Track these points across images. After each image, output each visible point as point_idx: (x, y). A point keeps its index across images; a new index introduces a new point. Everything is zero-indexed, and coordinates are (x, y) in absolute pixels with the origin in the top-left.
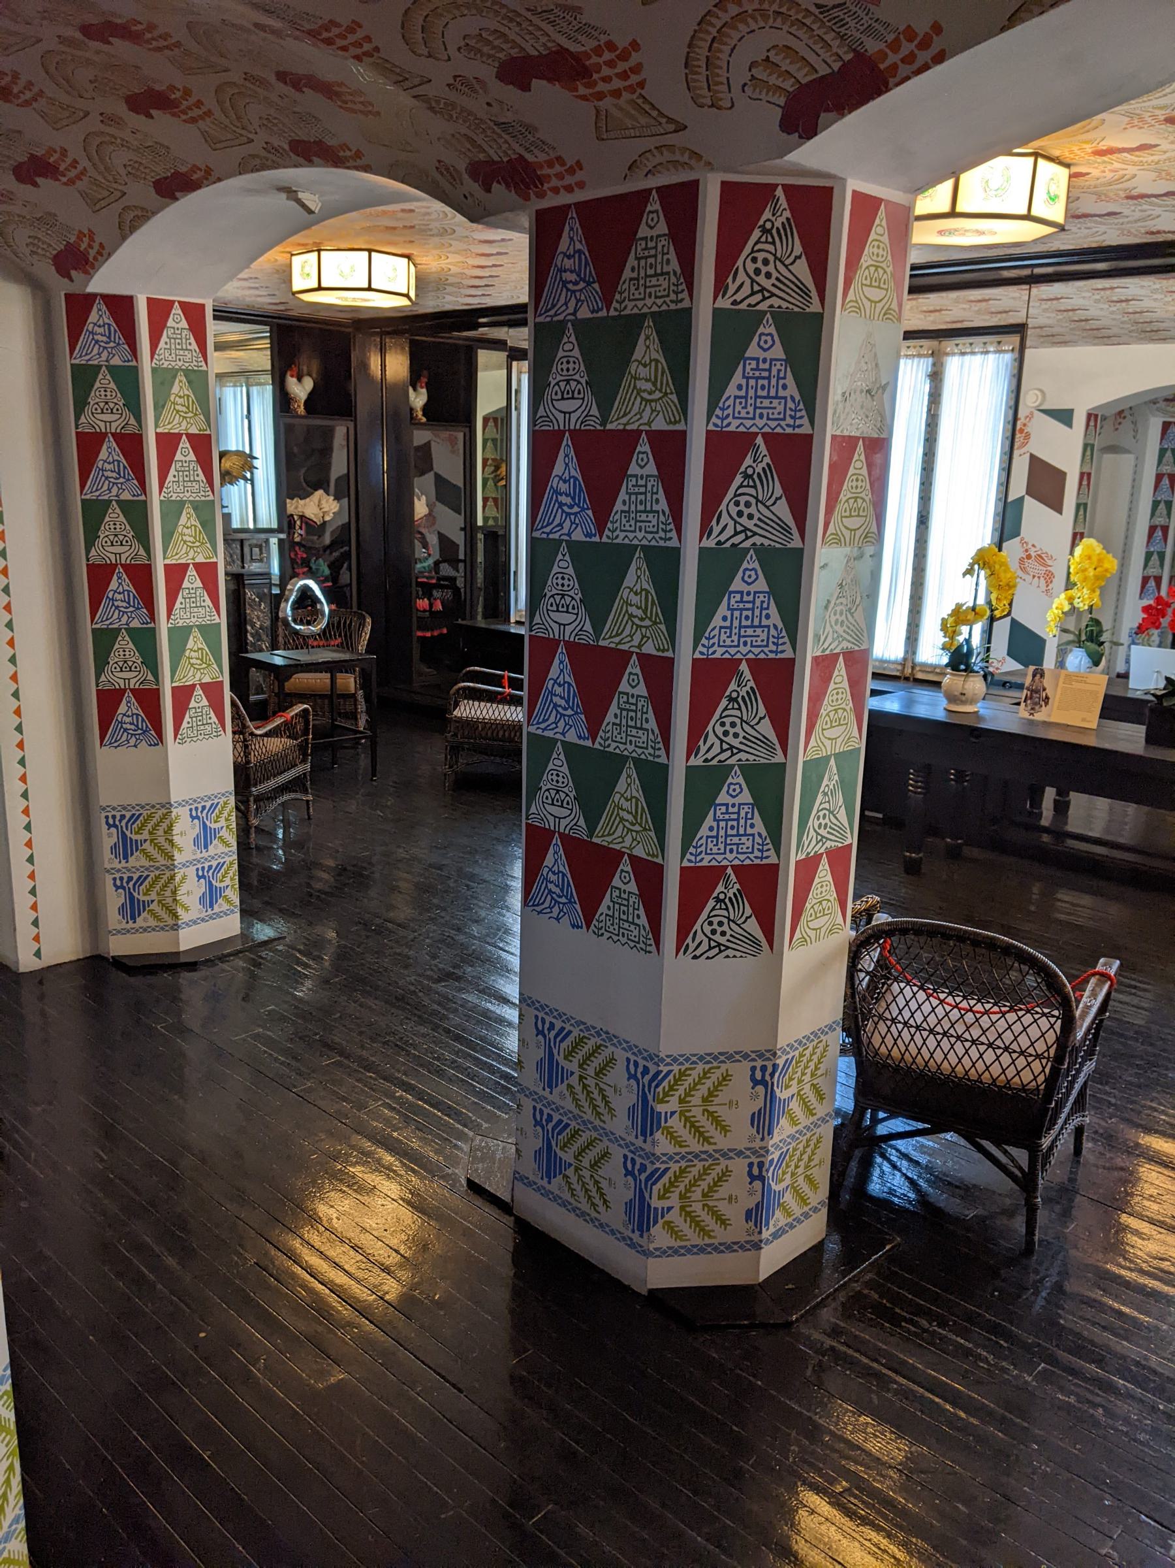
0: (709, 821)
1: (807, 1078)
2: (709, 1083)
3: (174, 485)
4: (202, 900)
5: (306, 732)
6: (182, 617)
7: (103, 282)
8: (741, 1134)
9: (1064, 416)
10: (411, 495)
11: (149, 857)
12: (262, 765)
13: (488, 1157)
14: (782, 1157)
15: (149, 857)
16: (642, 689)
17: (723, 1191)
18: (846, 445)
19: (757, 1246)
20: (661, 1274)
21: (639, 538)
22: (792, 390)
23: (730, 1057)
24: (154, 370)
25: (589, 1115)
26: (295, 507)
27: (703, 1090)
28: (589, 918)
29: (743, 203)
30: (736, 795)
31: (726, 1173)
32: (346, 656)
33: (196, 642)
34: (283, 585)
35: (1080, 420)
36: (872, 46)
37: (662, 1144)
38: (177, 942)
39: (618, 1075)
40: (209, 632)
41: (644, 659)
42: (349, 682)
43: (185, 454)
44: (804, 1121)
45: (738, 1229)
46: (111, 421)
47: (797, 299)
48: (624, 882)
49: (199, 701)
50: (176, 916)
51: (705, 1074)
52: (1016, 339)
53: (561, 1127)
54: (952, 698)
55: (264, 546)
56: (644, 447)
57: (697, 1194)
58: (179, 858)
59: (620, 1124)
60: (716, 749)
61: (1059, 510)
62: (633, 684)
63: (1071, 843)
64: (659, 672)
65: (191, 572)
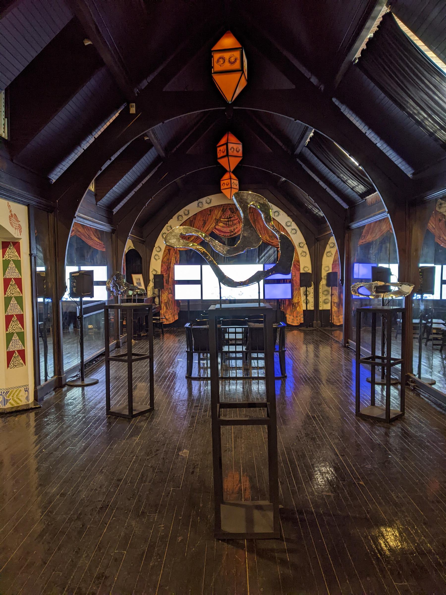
0: (10, 307)
2: (17, 392)
17: (20, 395)
27: (16, 394)
31: (20, 391)
47: (20, 330)
51: (16, 390)
57: (15, 396)
60: (9, 294)
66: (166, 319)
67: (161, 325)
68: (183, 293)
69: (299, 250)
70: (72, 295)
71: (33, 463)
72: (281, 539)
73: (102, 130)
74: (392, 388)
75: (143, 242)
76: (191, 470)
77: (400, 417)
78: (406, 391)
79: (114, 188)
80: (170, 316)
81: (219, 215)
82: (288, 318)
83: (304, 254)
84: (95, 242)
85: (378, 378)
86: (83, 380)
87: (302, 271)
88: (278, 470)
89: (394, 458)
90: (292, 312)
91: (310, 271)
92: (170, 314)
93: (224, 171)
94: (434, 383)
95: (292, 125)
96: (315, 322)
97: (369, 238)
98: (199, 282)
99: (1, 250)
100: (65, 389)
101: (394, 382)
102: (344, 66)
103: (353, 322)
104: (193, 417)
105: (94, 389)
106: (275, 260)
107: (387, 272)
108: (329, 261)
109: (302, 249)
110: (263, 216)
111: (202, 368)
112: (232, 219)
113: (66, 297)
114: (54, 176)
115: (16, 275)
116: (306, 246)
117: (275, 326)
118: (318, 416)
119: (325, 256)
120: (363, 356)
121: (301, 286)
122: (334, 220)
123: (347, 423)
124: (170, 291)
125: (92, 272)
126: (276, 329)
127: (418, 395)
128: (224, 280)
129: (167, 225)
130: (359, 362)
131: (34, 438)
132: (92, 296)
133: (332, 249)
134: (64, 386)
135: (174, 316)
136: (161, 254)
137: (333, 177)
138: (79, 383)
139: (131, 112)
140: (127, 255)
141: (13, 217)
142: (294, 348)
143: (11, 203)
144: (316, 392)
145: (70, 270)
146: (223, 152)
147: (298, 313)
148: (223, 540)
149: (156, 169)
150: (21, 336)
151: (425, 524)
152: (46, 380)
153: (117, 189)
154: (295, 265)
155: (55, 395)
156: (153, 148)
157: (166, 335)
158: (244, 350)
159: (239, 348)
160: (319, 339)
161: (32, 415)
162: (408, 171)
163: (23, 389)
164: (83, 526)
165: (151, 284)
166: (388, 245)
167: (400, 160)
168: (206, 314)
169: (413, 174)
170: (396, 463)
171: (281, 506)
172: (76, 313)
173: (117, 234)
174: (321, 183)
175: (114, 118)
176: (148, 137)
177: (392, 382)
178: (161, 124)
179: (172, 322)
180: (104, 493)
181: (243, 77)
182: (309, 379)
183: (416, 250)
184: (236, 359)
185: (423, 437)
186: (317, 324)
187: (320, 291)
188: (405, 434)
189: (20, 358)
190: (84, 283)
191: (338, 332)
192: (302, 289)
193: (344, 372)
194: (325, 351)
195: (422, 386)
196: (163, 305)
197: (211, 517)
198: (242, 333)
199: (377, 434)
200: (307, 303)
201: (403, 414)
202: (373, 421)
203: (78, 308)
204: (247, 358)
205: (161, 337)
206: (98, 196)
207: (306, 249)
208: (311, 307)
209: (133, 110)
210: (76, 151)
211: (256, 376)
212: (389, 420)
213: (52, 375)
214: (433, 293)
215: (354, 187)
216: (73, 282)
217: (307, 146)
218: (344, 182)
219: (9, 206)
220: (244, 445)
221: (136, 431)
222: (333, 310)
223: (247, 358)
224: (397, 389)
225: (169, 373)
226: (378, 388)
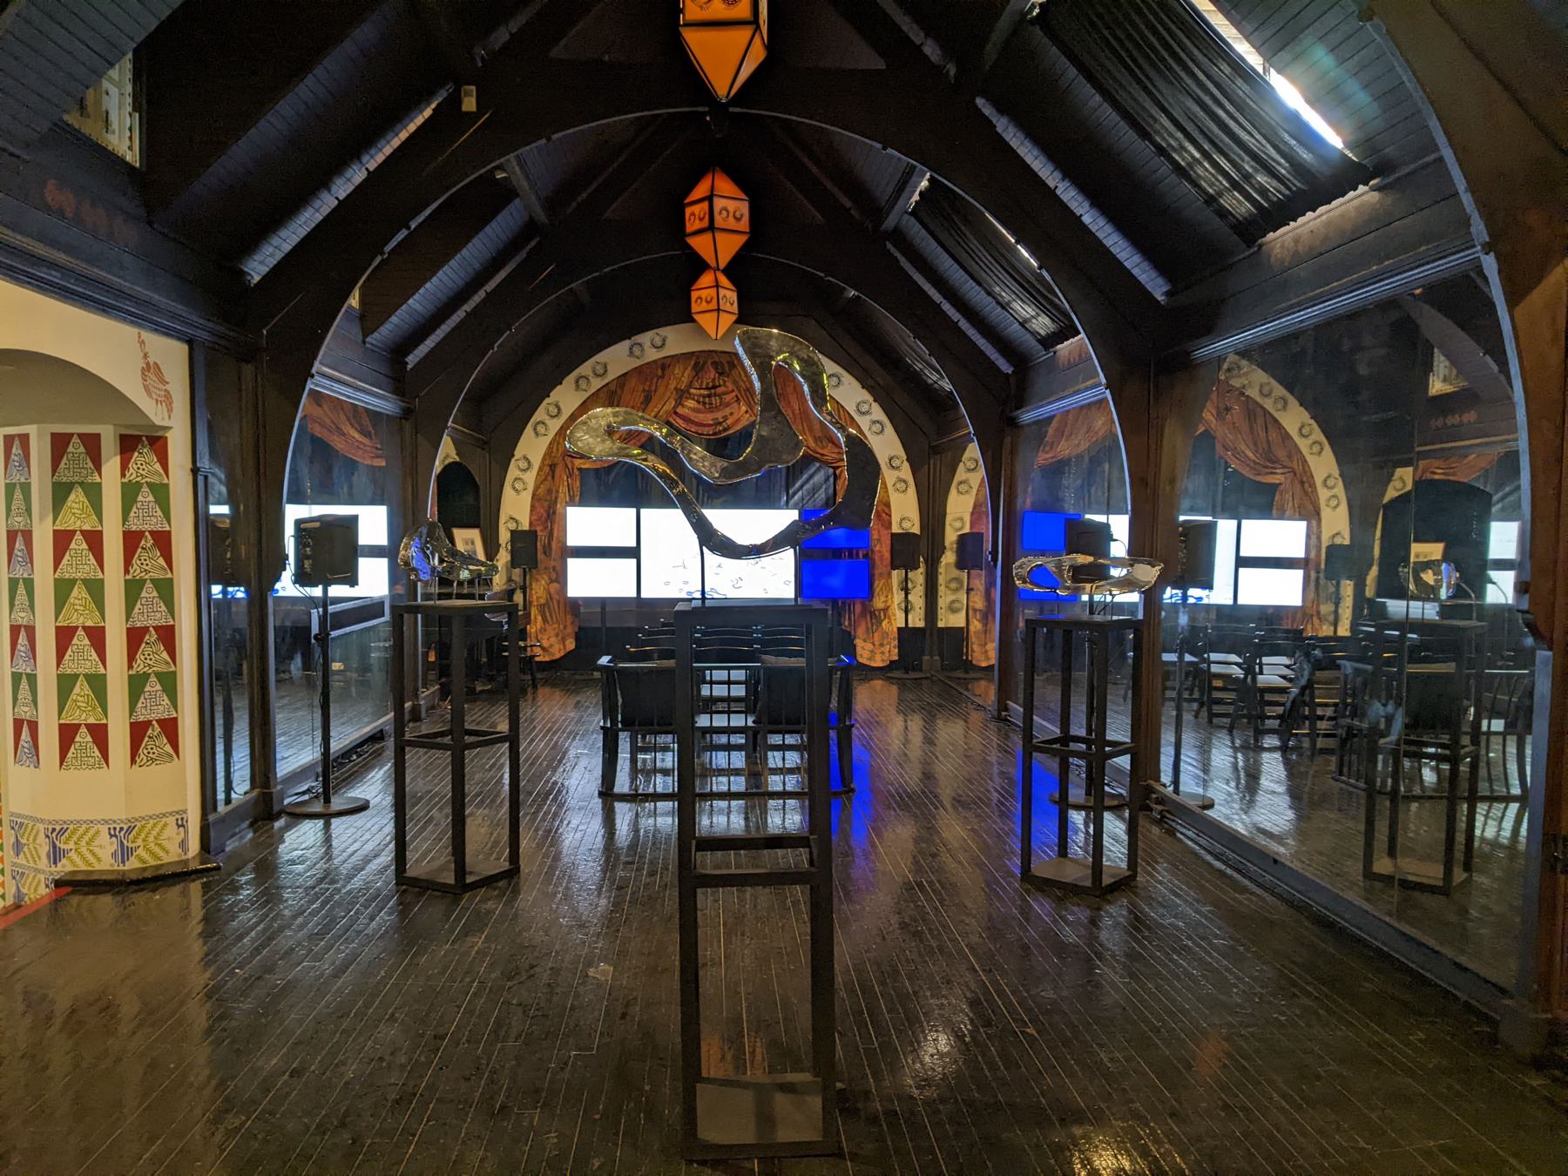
0: (138, 605)
31: (165, 825)
66: (543, 649)
67: (529, 664)
68: (588, 581)
69: (889, 476)
70: (301, 578)
71: (198, 1015)
72: (840, 1155)
73: (388, 150)
74: (1107, 816)
75: (483, 445)
76: (619, 1012)
77: (1125, 884)
78: (1142, 821)
79: (411, 301)
80: (553, 640)
81: (685, 380)
82: (859, 650)
83: (901, 486)
84: (352, 442)
85: (1077, 793)
86: (327, 801)
87: (895, 529)
88: (836, 1028)
89: (1111, 975)
90: (870, 632)
91: (916, 530)
92: (553, 633)
93: (698, 266)
94: (1211, 806)
95: (878, 161)
96: (926, 658)
97: (1064, 449)
98: (634, 553)
99: (118, 458)
100: (278, 824)
101: (1115, 803)
102: (1004, 24)
103: (1019, 659)
104: (620, 888)
105: (359, 823)
106: (828, 499)
107: (1104, 533)
108: (962, 507)
109: (896, 473)
110: (806, 388)
111: (642, 771)
112: (719, 390)
113: (286, 586)
114: (258, 267)
115: (155, 523)
116: (906, 465)
117: (831, 662)
118: (931, 883)
119: (953, 491)
120: (1040, 737)
121: (894, 568)
122: (973, 400)
123: (1000, 898)
124: (554, 576)
125: (354, 520)
126: (832, 671)
127: (1171, 832)
128: (711, 540)
129: (547, 400)
130: (1030, 746)
131: (197, 948)
132: (352, 581)
133: (970, 475)
134: (277, 816)
135: (563, 640)
136: (530, 478)
137: (975, 294)
138: (318, 807)
139: (464, 108)
140: (439, 477)
141: (151, 370)
142: (873, 723)
143: (147, 336)
144: (928, 833)
145: (294, 513)
146: (701, 220)
147: (885, 635)
148: (703, 1163)
149: (523, 254)
150: (169, 684)
151: (1173, 1115)
152: (228, 801)
153: (419, 303)
154: (878, 515)
155: (251, 840)
156: (517, 201)
157: (543, 692)
158: (750, 723)
159: (738, 721)
160: (935, 700)
161: (195, 888)
162: (1157, 287)
163: (171, 820)
164: (354, 1141)
165: (503, 557)
166: (1107, 466)
167: (1137, 258)
168: (650, 633)
169: (1168, 294)
170: (1113, 984)
171: (839, 1085)
172: (309, 629)
173: (414, 423)
174: (947, 307)
175: (419, 120)
176: (505, 171)
177: (1108, 802)
178: (543, 141)
179: (558, 656)
180: (402, 1067)
181: (757, 41)
182: (909, 797)
183: (1172, 481)
184: (728, 748)
185: (1177, 928)
186: (930, 660)
187: (941, 579)
188: (1137, 922)
190: (332, 551)
191: (983, 683)
192: (897, 576)
193: (997, 779)
194: (951, 731)
195: (1181, 810)
196: (534, 611)
197: (672, 1112)
198: (745, 683)
199: (1070, 925)
200: (907, 612)
201: (1133, 877)
202: (1063, 892)
203: (315, 614)
204: (755, 745)
205: (529, 696)
206: (368, 320)
207: (906, 472)
208: (917, 620)
209: (469, 104)
210: (317, 203)
211: (780, 788)
212: (1100, 889)
213: (246, 786)
214: (1209, 586)
215: (1026, 321)
216: (306, 545)
217: (914, 213)
218: (1003, 307)
219: (142, 343)
220: (750, 944)
221: (478, 922)
222: (972, 628)
223: (755, 745)
224: (1121, 818)
225: (555, 783)
226: (1077, 818)
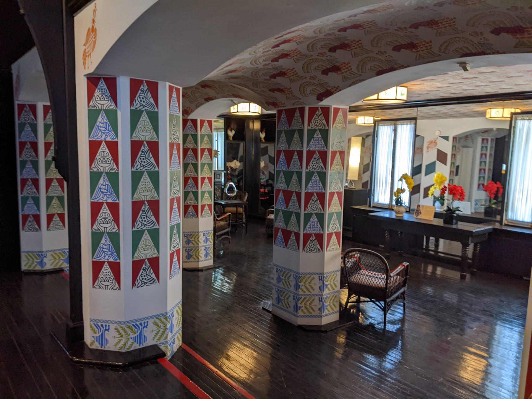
1: (332, 281)
3: (203, 159)
4: (205, 255)
5: (229, 220)
6: (204, 189)
7: (191, 117)
8: (317, 291)
9: (446, 138)
10: (260, 160)
11: (194, 244)
12: (219, 228)
13: (267, 304)
14: (326, 298)
15: (194, 244)
16: (296, 198)
17: (314, 303)
18: (334, 153)
19: (321, 317)
20: (301, 321)
21: (295, 170)
22: (323, 143)
23: (314, 274)
24: (201, 135)
25: (286, 288)
26: (229, 164)
27: (309, 280)
28: (286, 246)
29: (313, 111)
30: (314, 219)
31: (314, 300)
32: (241, 202)
33: (206, 195)
34: (225, 186)
35: (451, 139)
36: (329, 89)
37: (301, 292)
38: (198, 265)
39: (292, 278)
40: (209, 192)
41: (296, 192)
42: (241, 210)
43: (206, 153)
44: (332, 291)
45: (317, 313)
46: (191, 146)
48: (293, 237)
49: (206, 208)
50: (198, 259)
51: (309, 277)
52: (414, 121)
53: (281, 291)
54: (396, 213)
55: (220, 175)
56: (296, 153)
57: (308, 304)
58: (200, 245)
59: (292, 289)
61: (445, 164)
62: (294, 198)
63: (440, 254)
64: (299, 195)
65: (206, 179)
132: (340, 232)
163: (317, 277)
189: (323, 118)
